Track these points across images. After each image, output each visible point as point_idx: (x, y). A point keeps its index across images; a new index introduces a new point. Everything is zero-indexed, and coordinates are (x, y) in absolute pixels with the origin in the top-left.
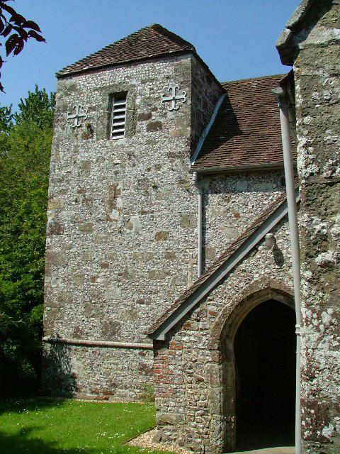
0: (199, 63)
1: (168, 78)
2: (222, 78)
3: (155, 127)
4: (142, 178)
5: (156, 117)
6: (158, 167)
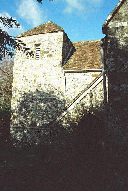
0: (65, 36)
1: (55, 39)
2: (72, 41)
3: (50, 56)
4: (45, 73)
5: (50, 53)
6: (51, 69)
